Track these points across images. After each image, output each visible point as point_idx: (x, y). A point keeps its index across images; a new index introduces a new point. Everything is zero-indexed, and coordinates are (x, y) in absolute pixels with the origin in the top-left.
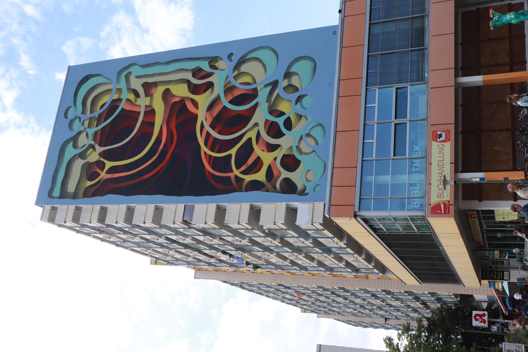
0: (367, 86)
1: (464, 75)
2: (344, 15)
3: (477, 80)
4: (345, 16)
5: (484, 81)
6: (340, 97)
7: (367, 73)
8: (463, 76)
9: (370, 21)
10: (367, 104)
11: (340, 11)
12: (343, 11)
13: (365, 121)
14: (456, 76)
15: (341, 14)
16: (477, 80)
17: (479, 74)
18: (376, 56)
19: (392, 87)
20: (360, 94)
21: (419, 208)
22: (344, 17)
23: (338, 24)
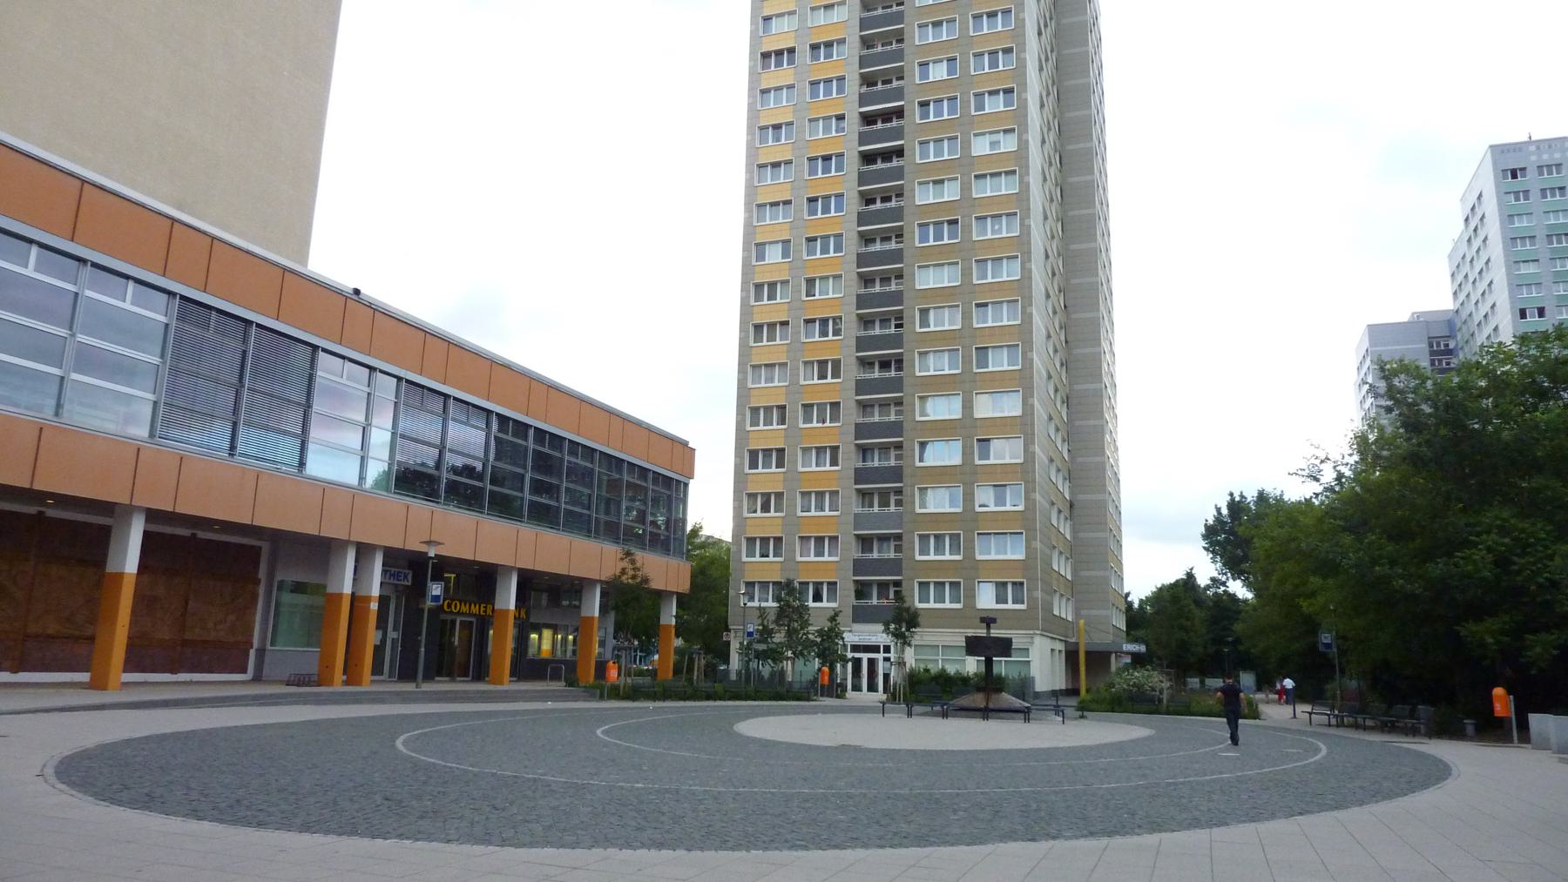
0: (183, 297)
1: (147, 535)
2: (220, 240)
3: (129, 557)
4: (83, 184)
5: (120, 575)
6: (173, 224)
7: (210, 308)
8: (145, 533)
9: (257, 323)
10: (137, 285)
11: (357, 292)
12: (355, 297)
13: (95, 265)
14: (152, 515)
15: (352, 292)
16: (129, 557)
17: (143, 567)
18: (245, 340)
19: (162, 356)
20: (280, 319)
21: (372, 488)
22: (347, 297)
23: (309, 267)
